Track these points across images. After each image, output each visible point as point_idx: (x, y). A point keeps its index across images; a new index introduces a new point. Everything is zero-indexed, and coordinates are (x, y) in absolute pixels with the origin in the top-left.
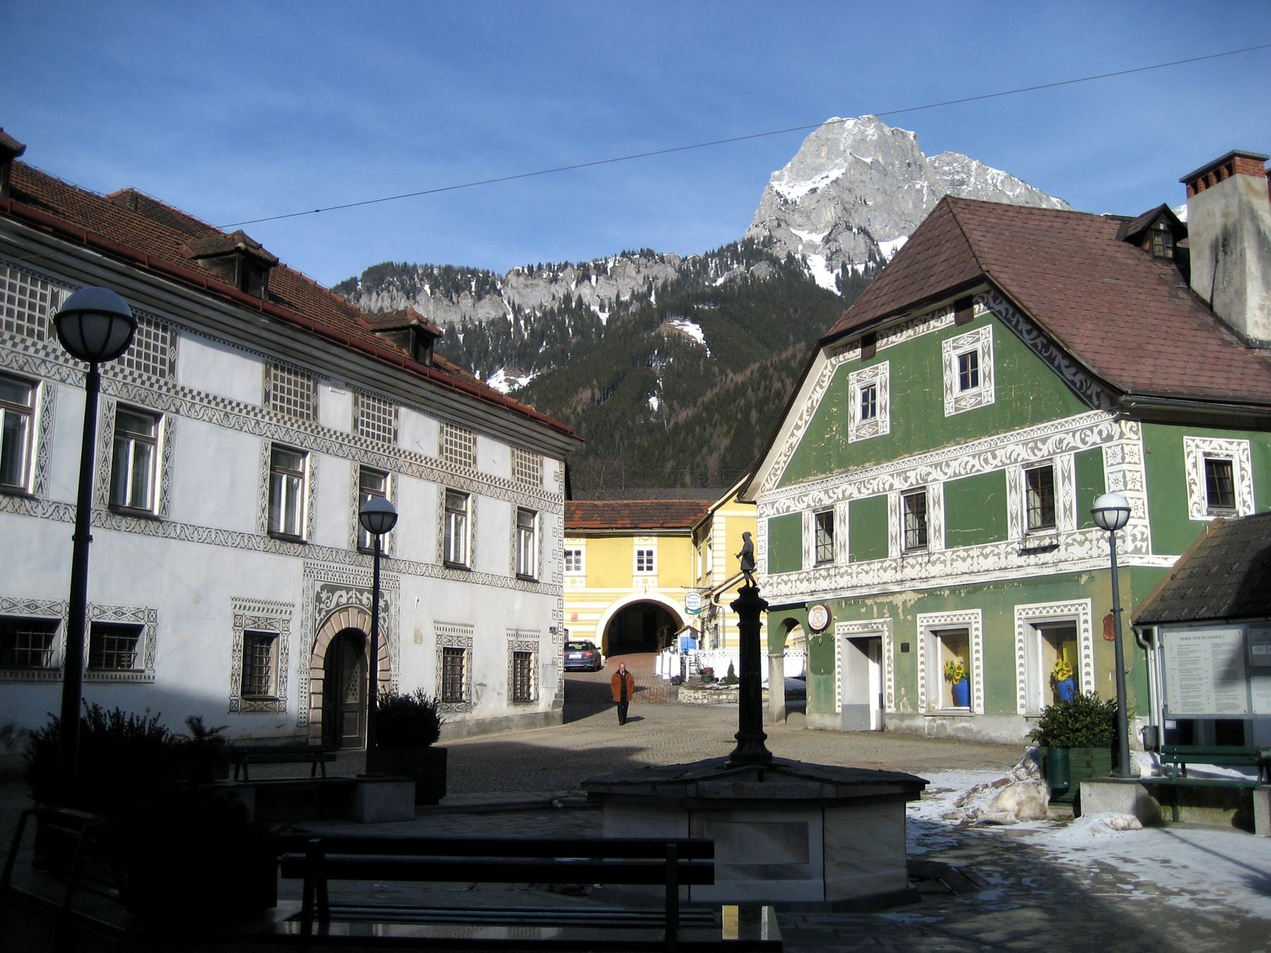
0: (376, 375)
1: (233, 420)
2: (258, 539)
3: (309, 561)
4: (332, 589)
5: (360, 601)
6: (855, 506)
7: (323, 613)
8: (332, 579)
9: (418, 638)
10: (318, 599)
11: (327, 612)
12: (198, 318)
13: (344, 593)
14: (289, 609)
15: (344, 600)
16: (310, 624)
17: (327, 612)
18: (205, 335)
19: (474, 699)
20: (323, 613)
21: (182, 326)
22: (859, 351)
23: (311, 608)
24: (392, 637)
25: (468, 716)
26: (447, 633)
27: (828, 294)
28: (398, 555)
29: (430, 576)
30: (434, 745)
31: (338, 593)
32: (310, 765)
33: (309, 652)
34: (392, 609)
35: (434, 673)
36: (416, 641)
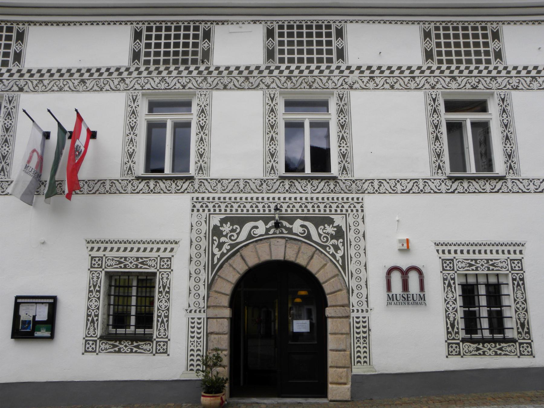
1: (90, 84)
24: (352, 267)
28: (361, 170)
34: (351, 235)
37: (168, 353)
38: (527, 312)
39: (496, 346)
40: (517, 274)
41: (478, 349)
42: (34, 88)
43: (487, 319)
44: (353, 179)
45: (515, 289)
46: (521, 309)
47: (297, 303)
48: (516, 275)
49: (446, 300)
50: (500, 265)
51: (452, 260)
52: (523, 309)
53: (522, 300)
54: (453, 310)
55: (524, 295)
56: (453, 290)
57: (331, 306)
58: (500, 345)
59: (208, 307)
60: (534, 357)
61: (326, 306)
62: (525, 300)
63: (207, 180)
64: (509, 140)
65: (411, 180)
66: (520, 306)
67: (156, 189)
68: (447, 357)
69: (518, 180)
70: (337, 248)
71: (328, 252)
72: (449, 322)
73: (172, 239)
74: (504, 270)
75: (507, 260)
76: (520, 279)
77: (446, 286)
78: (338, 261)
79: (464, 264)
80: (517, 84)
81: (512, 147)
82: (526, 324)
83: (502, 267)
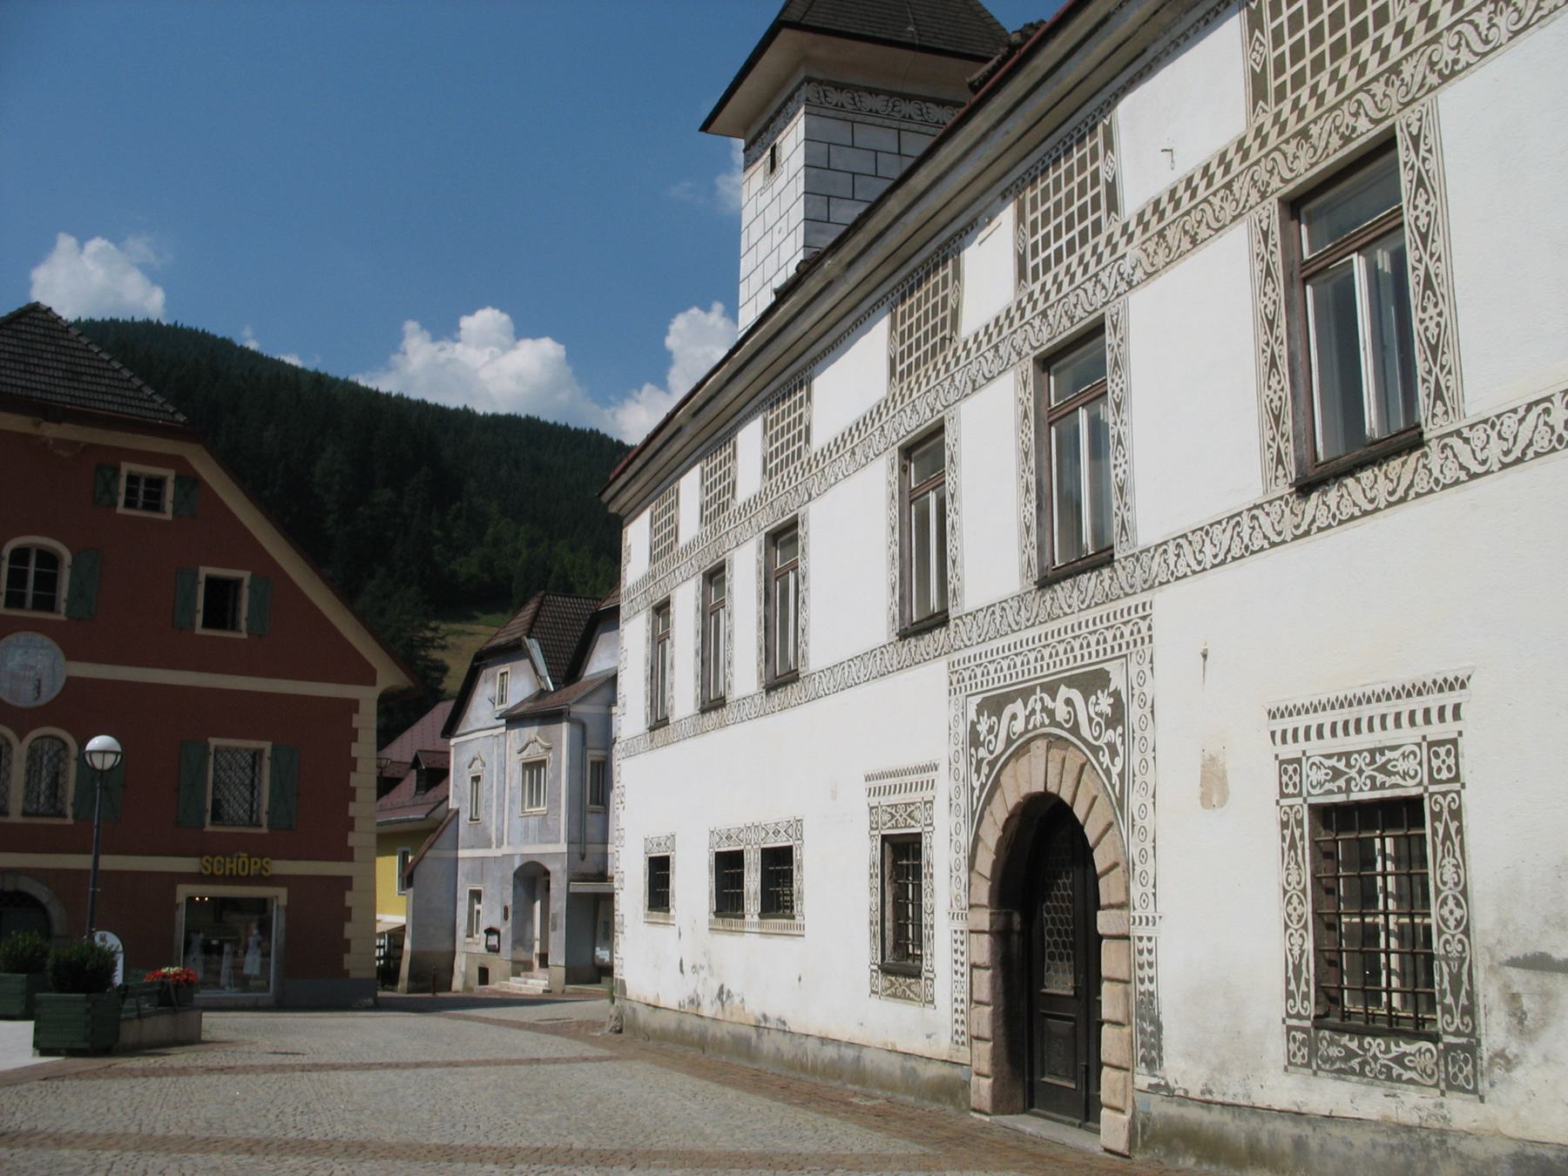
0: (1016, 125)
3: (956, 656)
4: (994, 705)
5: (1051, 713)
7: (985, 769)
8: (998, 682)
9: (1213, 785)
10: (975, 740)
11: (992, 764)
12: (813, 336)
14: (1449, 699)
15: (1019, 726)
16: (963, 801)
17: (992, 764)
18: (824, 353)
19: (1494, 1032)
20: (985, 769)
21: (804, 369)
24: (1135, 800)
25: (1461, 1112)
26: (1366, 740)
27: (111, 984)
29: (1249, 551)
32: (101, 867)
34: (1134, 713)
36: (1206, 801)
37: (1455, 735)
38: (1468, 936)
39: (1388, 1050)
41: (1350, 1054)
44: (1136, 551)
45: (1439, 848)
46: (1452, 923)
47: (1022, 923)
49: (1285, 892)
50: (1402, 766)
51: (1298, 761)
52: (1458, 923)
55: (1462, 873)
56: (1300, 859)
57: (1111, 906)
58: (1397, 1045)
59: (971, 906)
60: (1482, 1099)
61: (1098, 907)
62: (1464, 892)
63: (1458, 433)
65: (1529, 408)
66: (1451, 912)
67: (1484, 437)
68: (1286, 1069)
69: (1458, 433)
70: (1114, 753)
71: (1101, 764)
72: (1290, 960)
73: (924, 761)
74: (1410, 782)
75: (1419, 745)
76: (1451, 811)
77: (1286, 846)
78: (1113, 787)
79: (1324, 771)
80: (1453, 54)
81: (1440, 314)
82: (1465, 978)
83: (1405, 775)
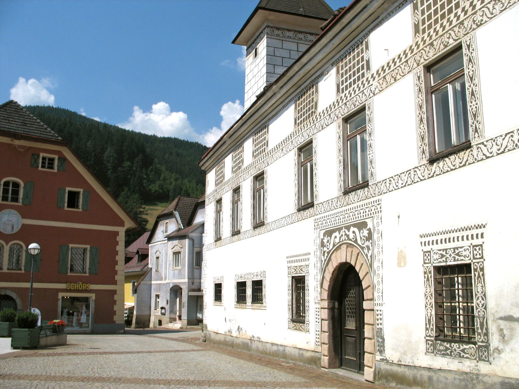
2: (295, 215)
4: (329, 233)
5: (348, 236)
6: (254, 282)
7: (326, 254)
9: (401, 260)
10: (323, 245)
11: (328, 253)
13: (336, 234)
15: (337, 240)
16: (319, 265)
17: (328, 253)
19: (495, 341)
20: (326, 254)
22: (459, 89)
23: (318, 253)
24: (376, 265)
25: (484, 368)
26: (452, 245)
30: (266, 37)
31: (334, 235)
33: (319, 286)
34: (375, 236)
35: (422, 301)
36: (399, 264)
38: (486, 310)
40: (478, 263)
41: (447, 349)
42: (492, 14)
43: (326, 310)
44: (376, 182)
45: (476, 281)
46: (481, 305)
48: (477, 264)
49: (425, 295)
50: (464, 253)
51: (430, 252)
52: (483, 305)
53: (482, 295)
54: (482, 307)
55: (484, 289)
56: (430, 284)
57: (368, 300)
58: (463, 346)
59: (321, 300)
60: (490, 364)
61: (363, 300)
62: (485, 295)
63: (483, 143)
64: (474, 95)
65: (506, 135)
66: (480, 302)
69: (483, 143)
71: (364, 253)
72: (427, 318)
74: (467, 259)
75: (470, 247)
77: (426, 280)
78: (368, 260)
81: (477, 104)
82: (485, 323)
83: (465, 256)
